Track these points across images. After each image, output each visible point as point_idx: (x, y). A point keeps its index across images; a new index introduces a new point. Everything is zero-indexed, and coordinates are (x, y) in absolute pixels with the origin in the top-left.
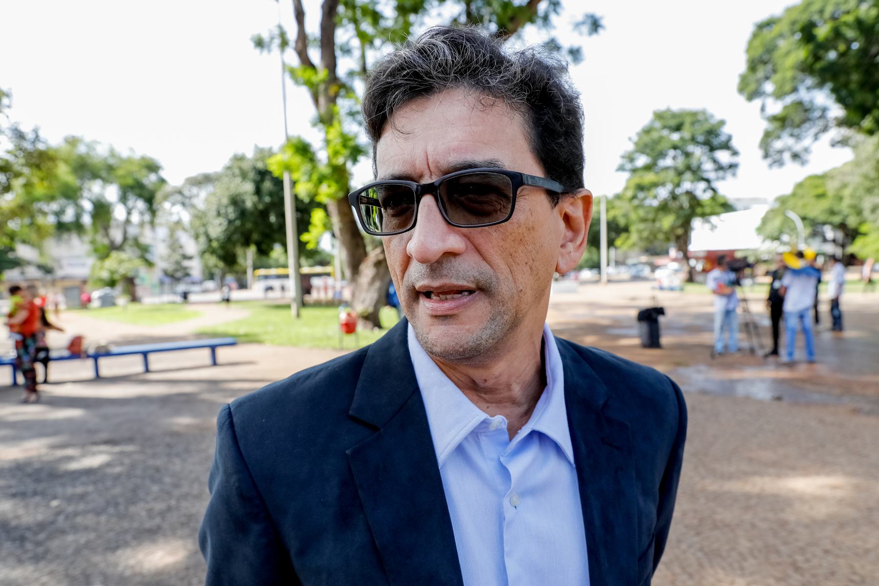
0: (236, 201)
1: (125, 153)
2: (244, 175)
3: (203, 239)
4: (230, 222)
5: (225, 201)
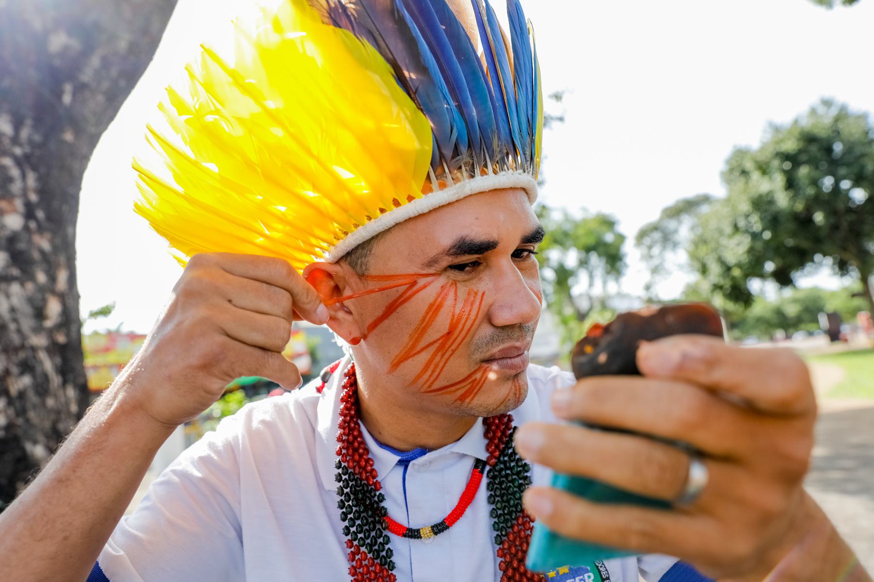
0: (762, 203)
1: (578, 215)
2: (764, 169)
3: (715, 269)
4: (755, 236)
5: (745, 206)
